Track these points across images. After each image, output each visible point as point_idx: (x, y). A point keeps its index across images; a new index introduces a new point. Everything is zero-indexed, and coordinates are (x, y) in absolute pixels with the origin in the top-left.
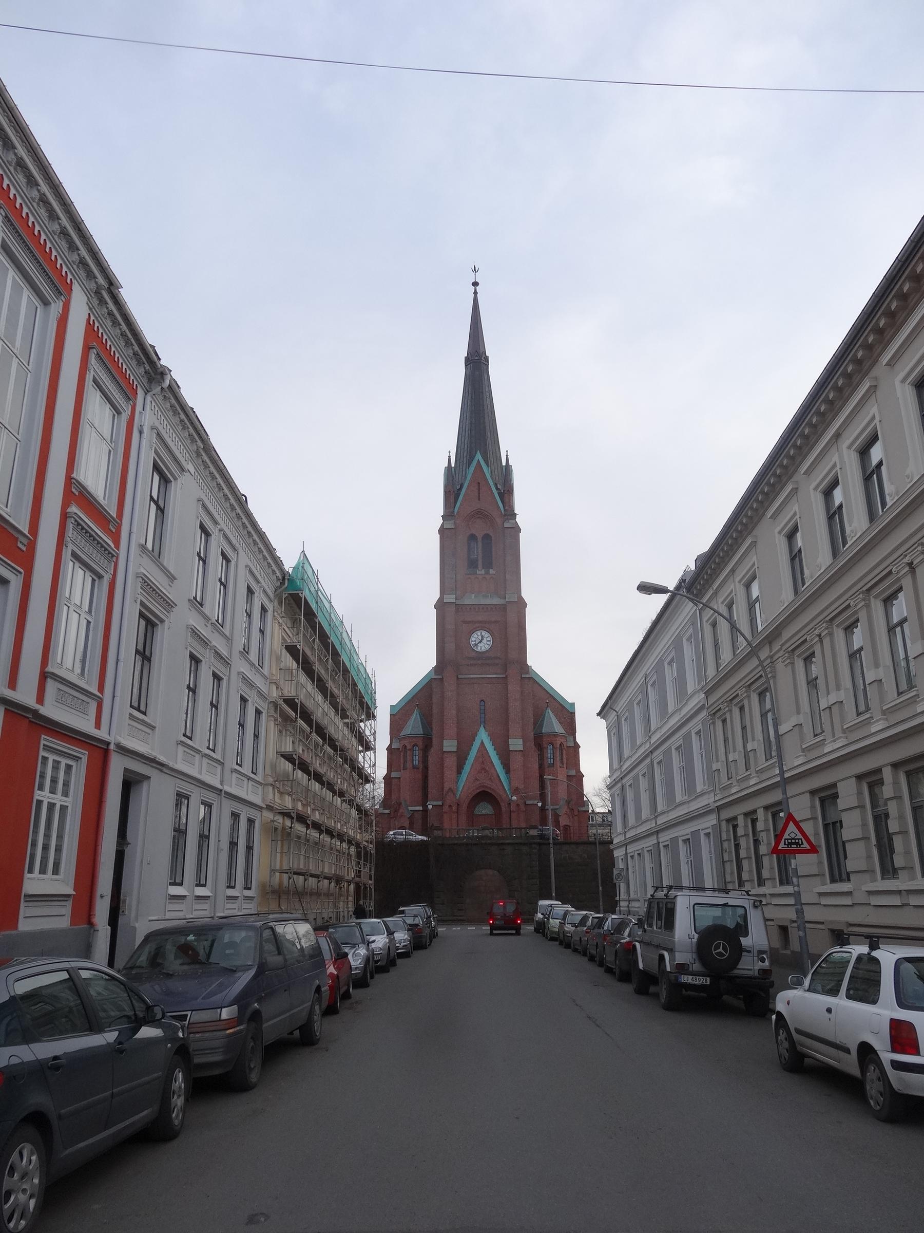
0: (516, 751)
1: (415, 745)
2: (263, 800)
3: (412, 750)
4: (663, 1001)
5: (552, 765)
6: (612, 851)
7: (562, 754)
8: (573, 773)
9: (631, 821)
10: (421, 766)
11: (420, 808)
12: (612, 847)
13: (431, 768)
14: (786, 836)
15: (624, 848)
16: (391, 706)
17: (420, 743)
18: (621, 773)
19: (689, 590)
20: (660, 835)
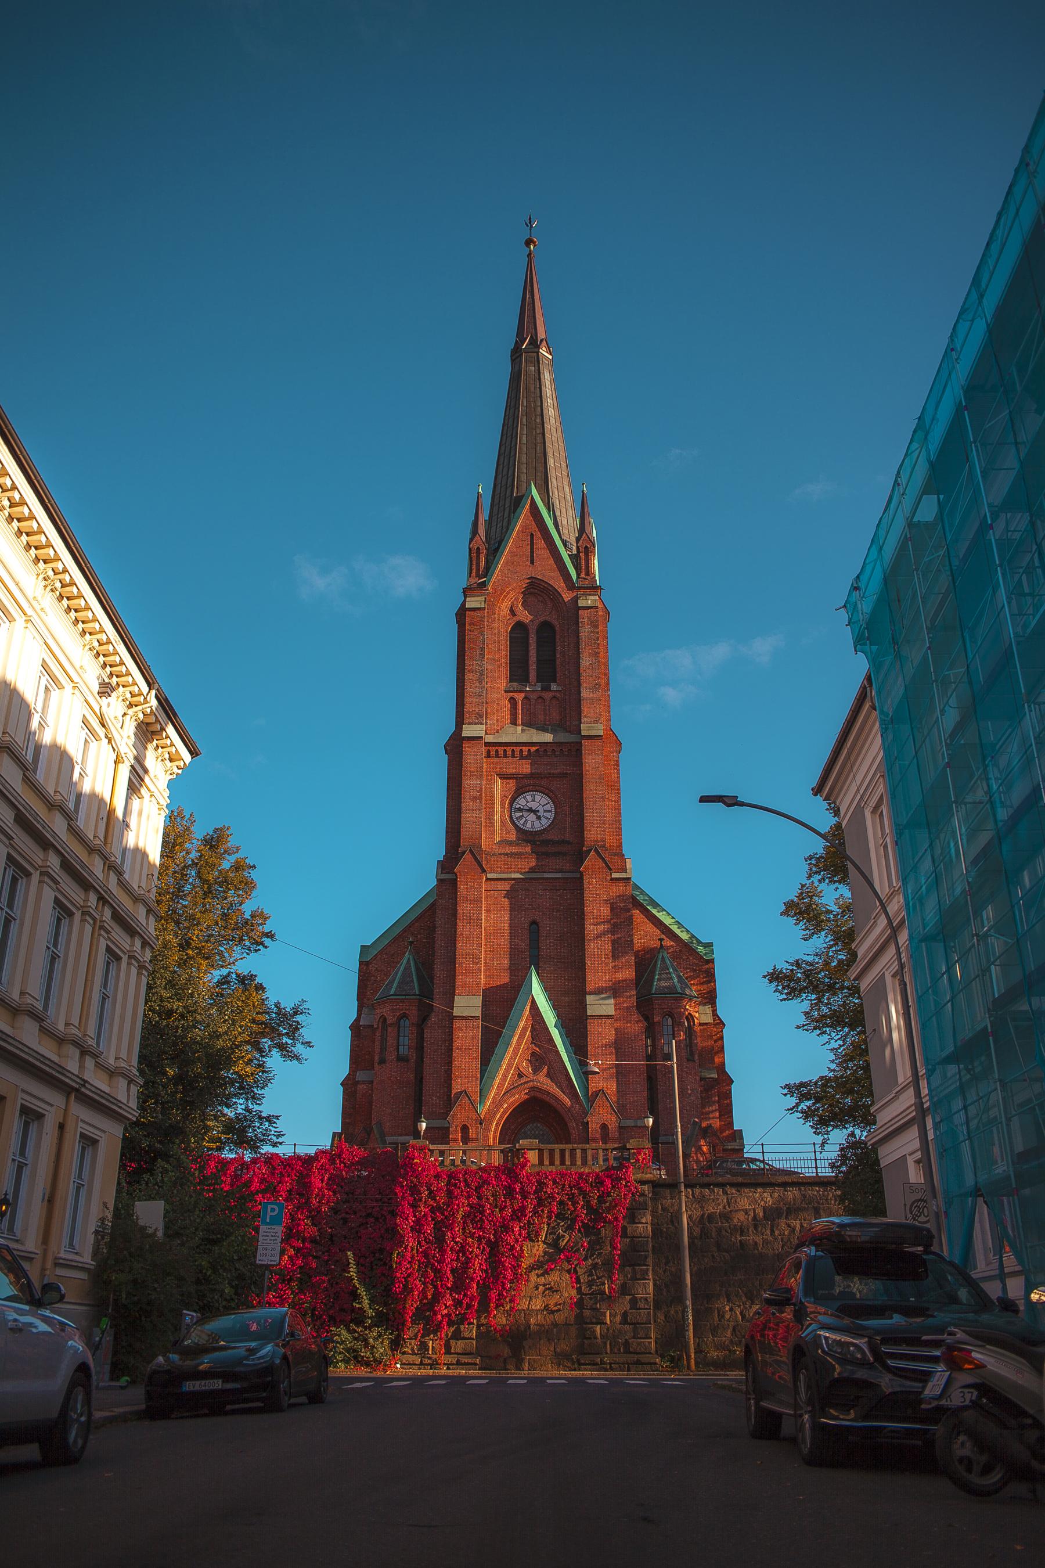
0: (601, 1017)
1: (404, 1016)
3: (397, 1024)
4: (806, 1451)
16: (362, 947)
17: (413, 1011)
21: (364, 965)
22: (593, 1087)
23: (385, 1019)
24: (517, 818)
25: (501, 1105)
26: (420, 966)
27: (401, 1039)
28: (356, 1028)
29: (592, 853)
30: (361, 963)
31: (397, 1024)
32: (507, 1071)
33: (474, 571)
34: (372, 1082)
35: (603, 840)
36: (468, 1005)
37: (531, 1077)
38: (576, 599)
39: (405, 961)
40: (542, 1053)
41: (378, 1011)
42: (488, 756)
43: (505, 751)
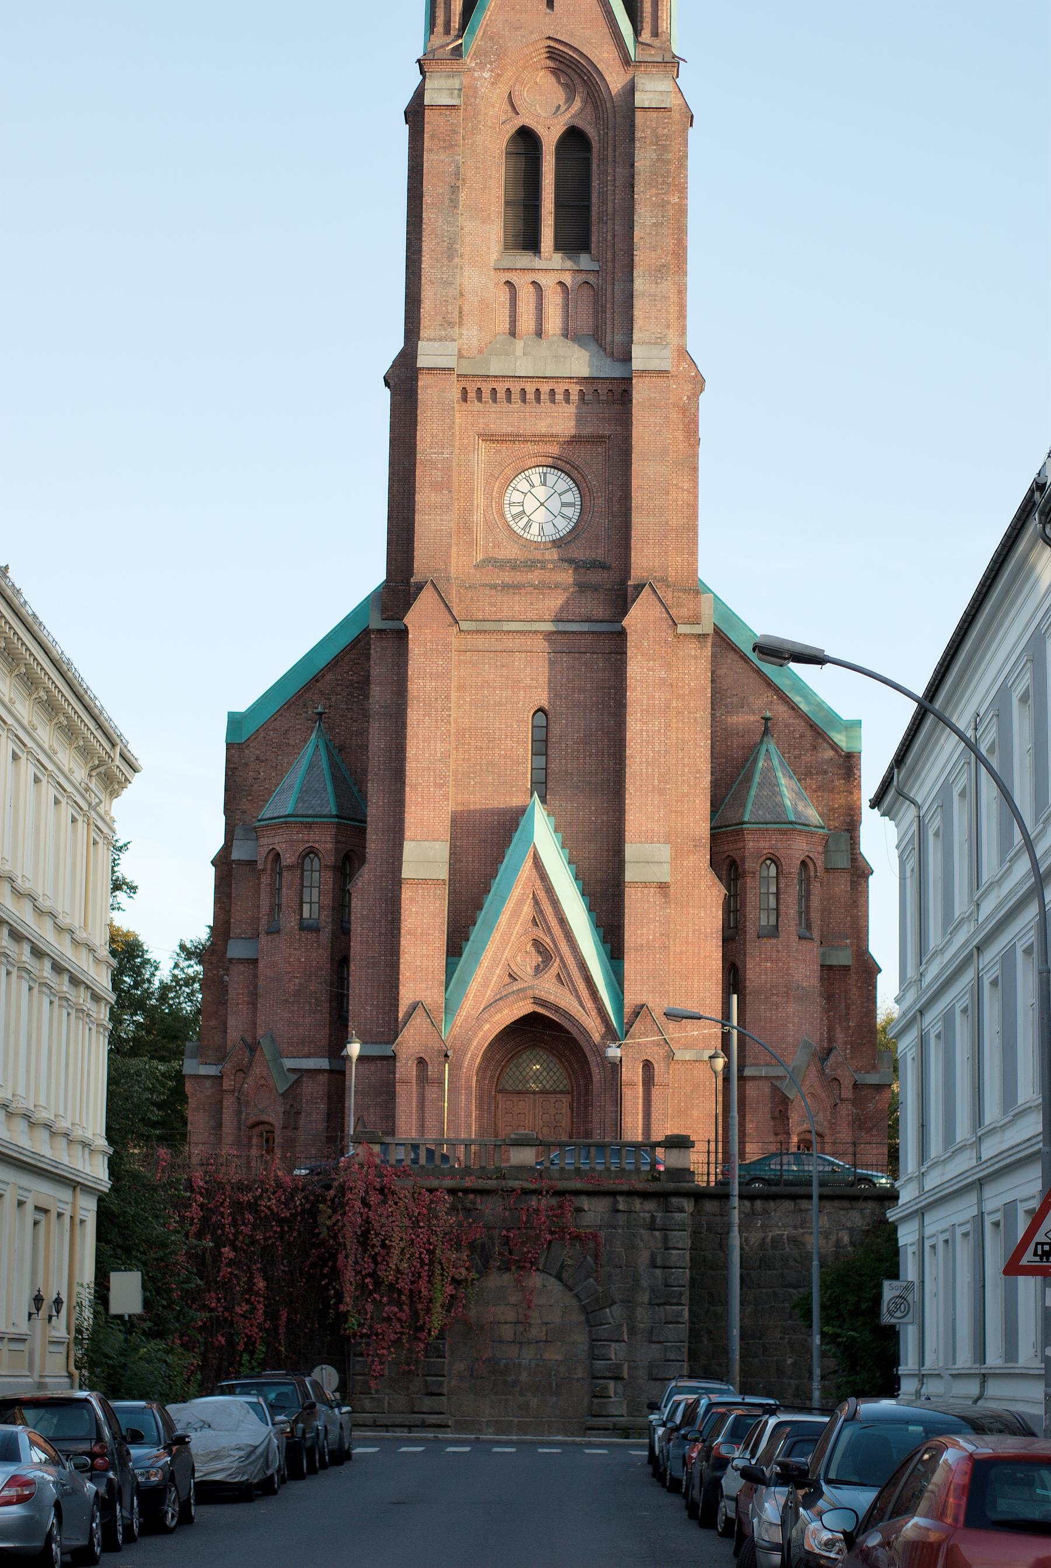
1: (311, 851)
5: (774, 932)
6: (893, 1229)
7: (805, 897)
8: (843, 958)
9: (992, 1113)
10: (326, 920)
11: (323, 1063)
12: (892, 1215)
13: (358, 929)
15: (972, 1198)
17: (325, 842)
18: (921, 992)
20: (928, 1219)
21: (235, 751)
23: (278, 855)
25: (480, 1027)
26: (335, 752)
27: (306, 891)
29: (646, 592)
30: (229, 746)
31: (300, 866)
32: (491, 969)
33: (440, 20)
34: (255, 961)
36: (426, 855)
38: (631, 90)
40: (549, 948)
41: (264, 841)
42: (465, 399)
43: (494, 391)
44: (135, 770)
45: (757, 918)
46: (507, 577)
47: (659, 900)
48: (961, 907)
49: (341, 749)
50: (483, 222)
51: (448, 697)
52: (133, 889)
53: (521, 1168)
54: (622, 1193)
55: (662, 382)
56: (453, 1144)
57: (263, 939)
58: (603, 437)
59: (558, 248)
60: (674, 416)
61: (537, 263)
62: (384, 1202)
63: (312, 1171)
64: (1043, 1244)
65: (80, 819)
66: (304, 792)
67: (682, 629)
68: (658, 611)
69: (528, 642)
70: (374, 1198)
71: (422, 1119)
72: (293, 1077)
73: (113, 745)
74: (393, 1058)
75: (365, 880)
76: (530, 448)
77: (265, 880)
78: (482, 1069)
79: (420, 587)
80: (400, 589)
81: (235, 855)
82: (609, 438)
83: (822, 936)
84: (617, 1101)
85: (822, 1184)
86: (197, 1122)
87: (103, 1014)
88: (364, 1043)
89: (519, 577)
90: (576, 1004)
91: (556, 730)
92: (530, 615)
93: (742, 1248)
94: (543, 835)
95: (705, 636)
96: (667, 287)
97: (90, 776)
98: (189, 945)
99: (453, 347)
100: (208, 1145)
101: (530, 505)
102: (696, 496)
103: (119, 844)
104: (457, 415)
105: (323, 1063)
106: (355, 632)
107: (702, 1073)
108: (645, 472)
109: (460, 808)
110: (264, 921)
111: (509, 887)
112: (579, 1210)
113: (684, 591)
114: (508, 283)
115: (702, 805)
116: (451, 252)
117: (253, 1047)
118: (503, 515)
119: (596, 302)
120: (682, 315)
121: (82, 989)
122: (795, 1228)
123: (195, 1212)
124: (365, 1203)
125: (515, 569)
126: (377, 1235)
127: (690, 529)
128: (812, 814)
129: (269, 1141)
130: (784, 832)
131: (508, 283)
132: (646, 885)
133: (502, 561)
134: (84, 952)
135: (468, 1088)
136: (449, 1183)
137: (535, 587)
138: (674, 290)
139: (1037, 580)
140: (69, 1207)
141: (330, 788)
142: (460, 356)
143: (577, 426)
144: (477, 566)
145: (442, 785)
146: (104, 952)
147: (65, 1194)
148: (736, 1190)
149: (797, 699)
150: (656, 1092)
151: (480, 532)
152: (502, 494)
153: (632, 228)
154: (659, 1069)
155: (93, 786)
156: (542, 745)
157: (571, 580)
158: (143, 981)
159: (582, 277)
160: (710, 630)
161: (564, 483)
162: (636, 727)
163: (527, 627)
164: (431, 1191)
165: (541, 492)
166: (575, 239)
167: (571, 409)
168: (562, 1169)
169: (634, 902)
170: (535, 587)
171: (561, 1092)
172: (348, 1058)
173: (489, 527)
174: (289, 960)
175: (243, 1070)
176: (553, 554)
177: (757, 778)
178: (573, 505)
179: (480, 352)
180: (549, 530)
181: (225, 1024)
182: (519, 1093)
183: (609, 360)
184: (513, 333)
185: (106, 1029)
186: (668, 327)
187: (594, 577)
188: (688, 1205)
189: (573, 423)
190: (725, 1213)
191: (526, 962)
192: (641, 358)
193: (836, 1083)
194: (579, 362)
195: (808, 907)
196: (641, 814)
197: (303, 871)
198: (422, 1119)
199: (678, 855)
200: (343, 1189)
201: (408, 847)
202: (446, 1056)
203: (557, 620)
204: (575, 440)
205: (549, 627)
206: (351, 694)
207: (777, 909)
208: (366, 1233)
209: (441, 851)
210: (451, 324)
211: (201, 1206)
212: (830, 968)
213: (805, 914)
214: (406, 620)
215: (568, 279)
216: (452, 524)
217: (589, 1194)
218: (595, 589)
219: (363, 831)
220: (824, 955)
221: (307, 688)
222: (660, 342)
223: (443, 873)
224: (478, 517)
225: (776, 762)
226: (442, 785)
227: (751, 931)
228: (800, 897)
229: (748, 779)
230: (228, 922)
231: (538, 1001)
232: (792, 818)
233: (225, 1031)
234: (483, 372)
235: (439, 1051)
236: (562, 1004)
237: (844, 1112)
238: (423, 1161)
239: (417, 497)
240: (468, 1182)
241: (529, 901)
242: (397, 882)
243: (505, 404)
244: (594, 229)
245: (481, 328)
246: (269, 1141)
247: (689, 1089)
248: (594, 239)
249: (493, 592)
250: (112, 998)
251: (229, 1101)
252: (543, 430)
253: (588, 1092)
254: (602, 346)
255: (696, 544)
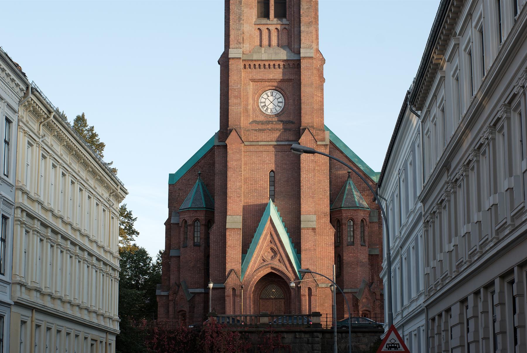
1: (197, 220)
2: (11, 297)
7: (363, 232)
8: (376, 252)
9: (406, 303)
11: (202, 290)
14: (388, 342)
16: (170, 174)
17: (202, 216)
19: (412, 103)
21: (171, 186)
22: (304, 267)
23: (186, 221)
24: (262, 107)
25: (253, 277)
27: (196, 233)
28: (168, 224)
29: (306, 131)
30: (170, 185)
31: (193, 225)
32: (257, 258)
34: (179, 257)
35: (313, 123)
36: (234, 220)
37: (270, 262)
39: (196, 186)
40: (276, 249)
41: (181, 217)
42: (245, 68)
44: (127, 194)
45: (347, 239)
46: (260, 127)
47: (313, 234)
48: (397, 233)
49: (207, 185)
50: (250, 9)
51: (241, 167)
52: (138, 233)
53: (264, 324)
54: (297, 332)
55: (310, 60)
56: (246, 317)
57: (182, 249)
58: (291, 79)
59: (275, 17)
60: (315, 72)
61: (268, 22)
62: (218, 336)
63: (194, 326)
64: (389, 344)
65: (106, 210)
66: (195, 200)
67: (319, 143)
68: (311, 137)
69: (267, 148)
70: (215, 335)
71: (234, 308)
72: (192, 295)
73: (118, 185)
74: (224, 288)
75: (215, 228)
76: (267, 83)
77: (182, 229)
78: (254, 291)
79: (231, 131)
80: (225, 131)
81: (172, 221)
82: (294, 79)
83: (369, 245)
84: (300, 301)
85: (353, 328)
86: (161, 311)
87: (117, 275)
88: (214, 283)
89: (264, 127)
90: (285, 269)
91: (277, 177)
92: (268, 139)
93: (338, 350)
94: (273, 213)
95: (327, 145)
96: (312, 29)
97: (110, 196)
98: (162, 252)
99: (241, 51)
100: (165, 318)
101: (267, 102)
102: (323, 99)
103: (133, 218)
104: (243, 73)
105: (202, 290)
106: (211, 146)
107: (328, 291)
108: (305, 90)
109: (246, 204)
110: (182, 243)
111: (263, 230)
112: (283, 338)
113: (319, 130)
114: (259, 29)
115: (327, 201)
116: (240, 19)
117: (179, 286)
118: (258, 106)
119: (288, 35)
120: (317, 38)
121: (108, 267)
122: (356, 342)
123: (155, 340)
124: (212, 336)
125: (263, 124)
126: (216, 347)
127: (321, 110)
128: (365, 204)
129: (184, 315)
130: (355, 210)
131: (259, 29)
132: (308, 229)
133: (258, 122)
134: (108, 254)
135: (250, 298)
136: (239, 329)
137: (270, 130)
138: (314, 30)
139: (413, 125)
140: (105, 339)
141: (203, 198)
142: (243, 54)
143: (283, 76)
144: (250, 123)
145: (239, 197)
146: (117, 254)
147: (103, 335)
148: (336, 330)
149: (359, 165)
150: (312, 298)
151: (251, 112)
152: (258, 99)
153: (300, 10)
154: (313, 290)
155: (111, 199)
156: (273, 182)
157: (281, 127)
158: (147, 264)
159: (283, 26)
160: (328, 143)
161: (279, 95)
162: (304, 176)
163: (267, 143)
164: (233, 332)
165: (271, 98)
166: (281, 14)
167: (281, 70)
168: (277, 324)
169: (305, 235)
170: (270, 130)
171: (281, 299)
172: (209, 288)
173: (254, 110)
174: (190, 256)
175: (176, 293)
176: (276, 119)
177: (346, 192)
178: (281, 102)
179: (250, 52)
180: (274, 111)
181: (170, 278)
182: (267, 299)
183: (293, 54)
184: (261, 46)
185: (118, 280)
186: (312, 42)
187: (289, 126)
188: (320, 336)
189: (281, 75)
190: (333, 338)
191: (269, 255)
192: (304, 53)
193: (374, 294)
194: (283, 55)
195: (364, 235)
196: (306, 205)
197: (194, 226)
198: (234, 308)
199: (319, 218)
200: (204, 332)
201: (228, 218)
202: (242, 287)
203: (277, 141)
204: (282, 81)
205: (275, 143)
206: (210, 167)
207: (353, 236)
208: (212, 347)
209: (240, 219)
210: (240, 43)
211: (157, 338)
212: (372, 255)
213: (363, 237)
214: (226, 142)
215: (279, 27)
216: (241, 110)
217: (287, 332)
218: (290, 130)
219: (213, 213)
220: (370, 251)
221: (195, 165)
222: (310, 47)
223: (240, 226)
224: (250, 107)
225: (352, 187)
226: (239, 197)
227: (345, 243)
228: (361, 232)
229: (343, 193)
230: (170, 244)
231: (272, 268)
232: (358, 205)
233: (169, 280)
234: (251, 59)
235: (240, 286)
236: (281, 269)
237: (377, 304)
238: (231, 322)
239: (230, 101)
240: (246, 329)
241: (269, 235)
242: (225, 229)
243: (259, 69)
244: (287, 10)
245: (250, 44)
246: (184, 315)
247: (324, 297)
248: (287, 13)
249: (256, 132)
250: (120, 270)
251: (171, 303)
252: (271, 78)
253: (290, 298)
254: (291, 49)
255: (323, 114)
